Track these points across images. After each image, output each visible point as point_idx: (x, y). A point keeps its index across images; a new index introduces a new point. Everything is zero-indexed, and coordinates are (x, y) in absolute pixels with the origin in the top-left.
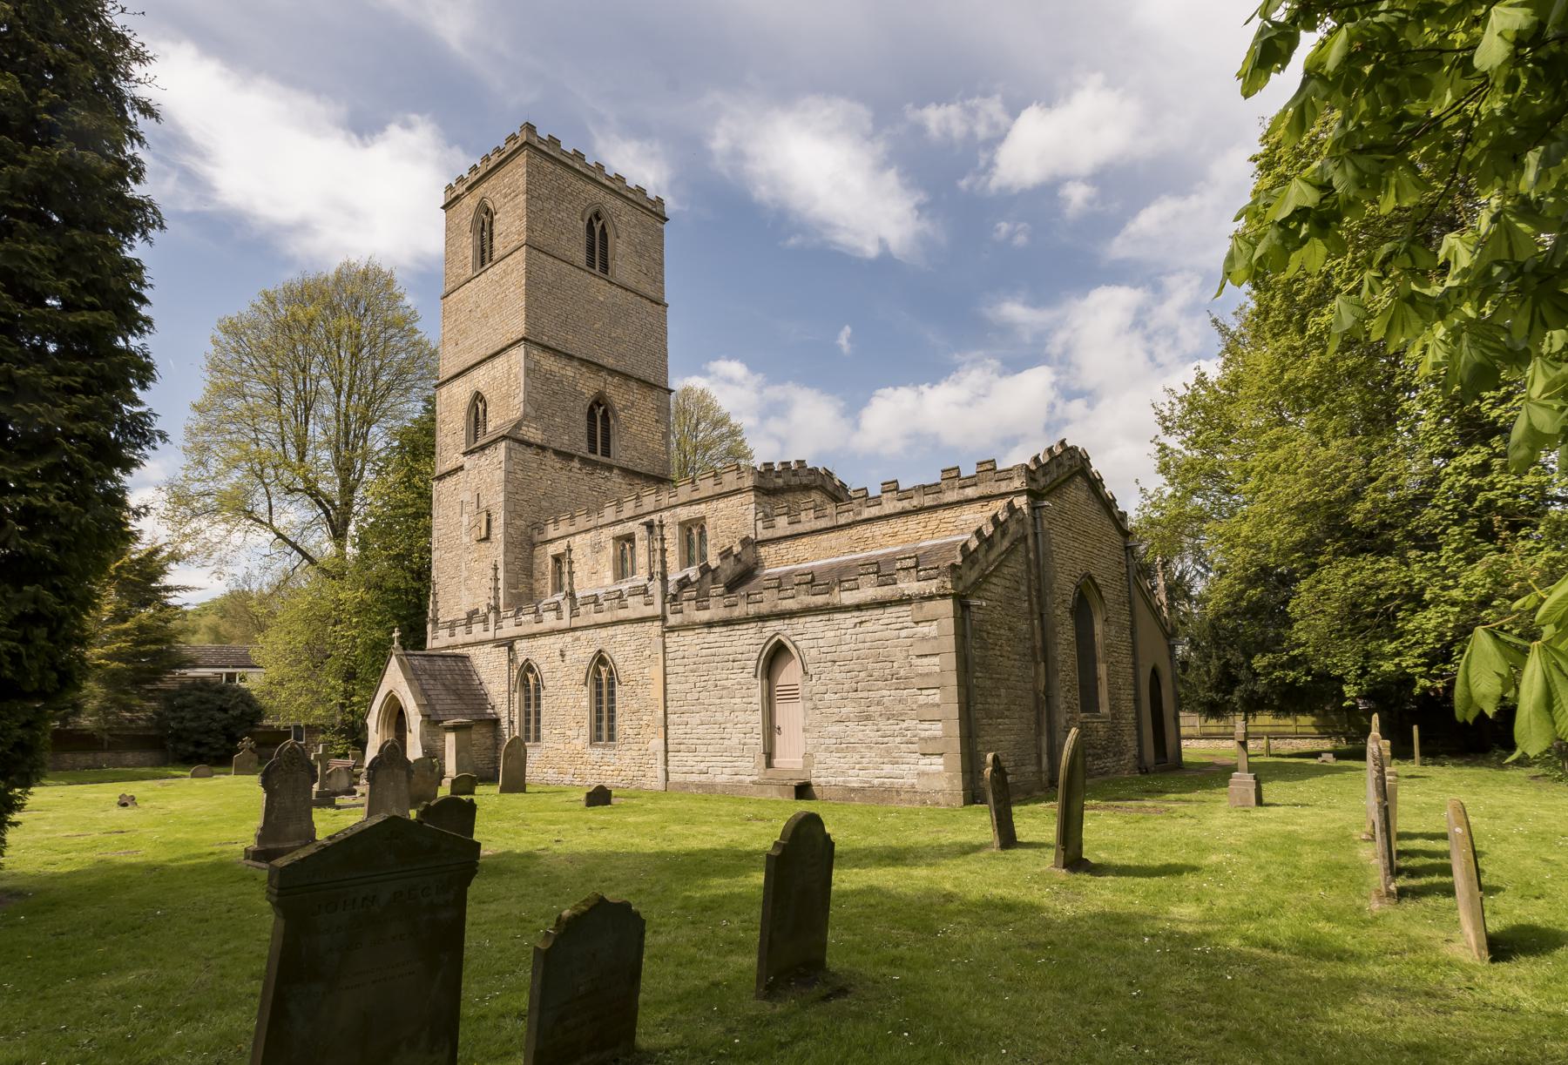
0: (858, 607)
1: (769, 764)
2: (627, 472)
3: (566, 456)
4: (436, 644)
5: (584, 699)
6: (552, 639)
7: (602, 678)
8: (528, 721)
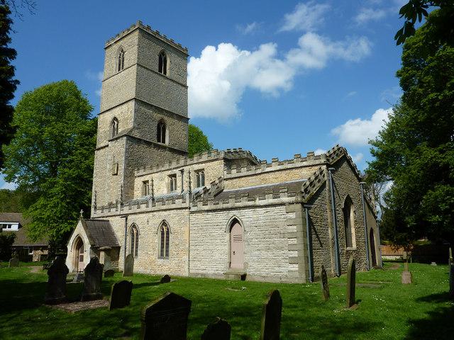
2: (172, 150)
4: (95, 216)
5: (157, 240)
6: (144, 215)
7: (165, 232)
8: (132, 248)
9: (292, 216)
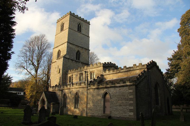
0: (120, 87)
3: (73, 60)
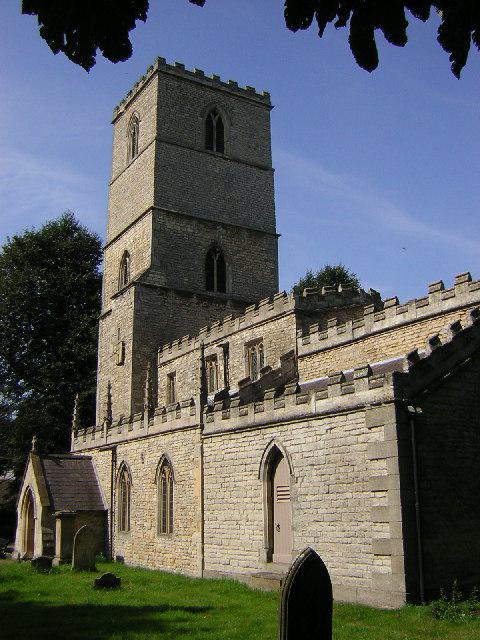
0: (327, 414)
1: (270, 559)
3: (185, 295)
9: (378, 435)
